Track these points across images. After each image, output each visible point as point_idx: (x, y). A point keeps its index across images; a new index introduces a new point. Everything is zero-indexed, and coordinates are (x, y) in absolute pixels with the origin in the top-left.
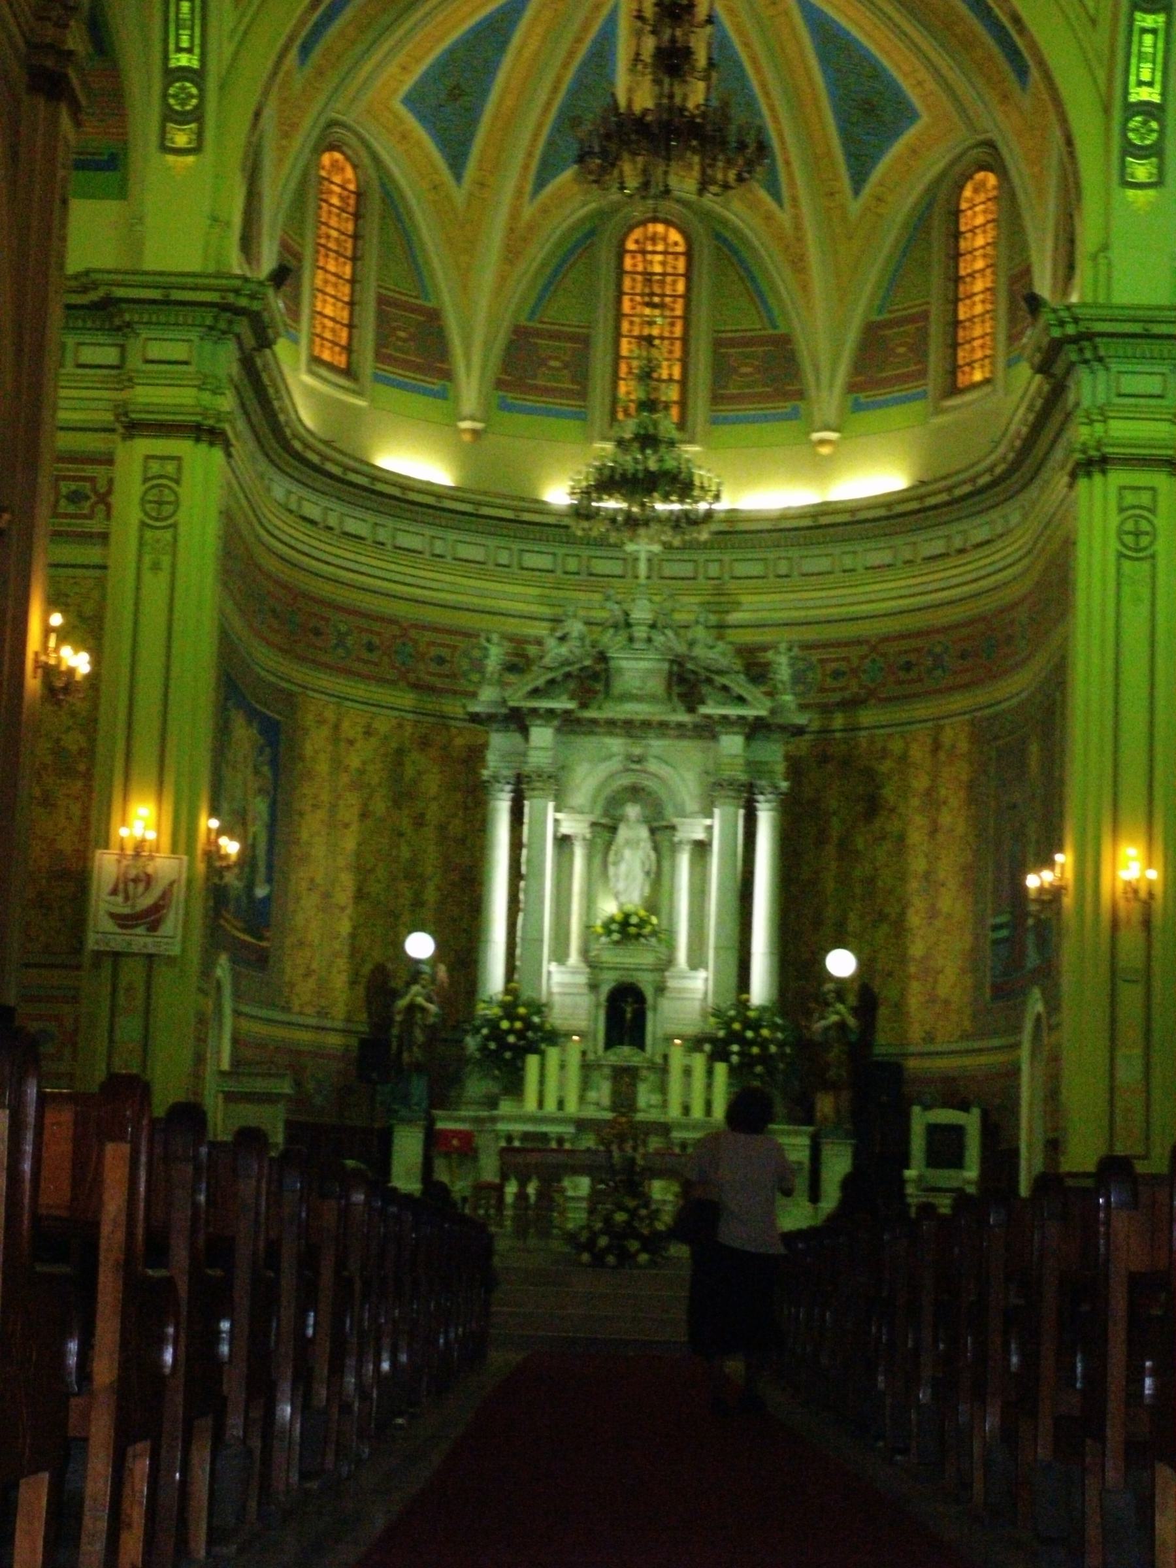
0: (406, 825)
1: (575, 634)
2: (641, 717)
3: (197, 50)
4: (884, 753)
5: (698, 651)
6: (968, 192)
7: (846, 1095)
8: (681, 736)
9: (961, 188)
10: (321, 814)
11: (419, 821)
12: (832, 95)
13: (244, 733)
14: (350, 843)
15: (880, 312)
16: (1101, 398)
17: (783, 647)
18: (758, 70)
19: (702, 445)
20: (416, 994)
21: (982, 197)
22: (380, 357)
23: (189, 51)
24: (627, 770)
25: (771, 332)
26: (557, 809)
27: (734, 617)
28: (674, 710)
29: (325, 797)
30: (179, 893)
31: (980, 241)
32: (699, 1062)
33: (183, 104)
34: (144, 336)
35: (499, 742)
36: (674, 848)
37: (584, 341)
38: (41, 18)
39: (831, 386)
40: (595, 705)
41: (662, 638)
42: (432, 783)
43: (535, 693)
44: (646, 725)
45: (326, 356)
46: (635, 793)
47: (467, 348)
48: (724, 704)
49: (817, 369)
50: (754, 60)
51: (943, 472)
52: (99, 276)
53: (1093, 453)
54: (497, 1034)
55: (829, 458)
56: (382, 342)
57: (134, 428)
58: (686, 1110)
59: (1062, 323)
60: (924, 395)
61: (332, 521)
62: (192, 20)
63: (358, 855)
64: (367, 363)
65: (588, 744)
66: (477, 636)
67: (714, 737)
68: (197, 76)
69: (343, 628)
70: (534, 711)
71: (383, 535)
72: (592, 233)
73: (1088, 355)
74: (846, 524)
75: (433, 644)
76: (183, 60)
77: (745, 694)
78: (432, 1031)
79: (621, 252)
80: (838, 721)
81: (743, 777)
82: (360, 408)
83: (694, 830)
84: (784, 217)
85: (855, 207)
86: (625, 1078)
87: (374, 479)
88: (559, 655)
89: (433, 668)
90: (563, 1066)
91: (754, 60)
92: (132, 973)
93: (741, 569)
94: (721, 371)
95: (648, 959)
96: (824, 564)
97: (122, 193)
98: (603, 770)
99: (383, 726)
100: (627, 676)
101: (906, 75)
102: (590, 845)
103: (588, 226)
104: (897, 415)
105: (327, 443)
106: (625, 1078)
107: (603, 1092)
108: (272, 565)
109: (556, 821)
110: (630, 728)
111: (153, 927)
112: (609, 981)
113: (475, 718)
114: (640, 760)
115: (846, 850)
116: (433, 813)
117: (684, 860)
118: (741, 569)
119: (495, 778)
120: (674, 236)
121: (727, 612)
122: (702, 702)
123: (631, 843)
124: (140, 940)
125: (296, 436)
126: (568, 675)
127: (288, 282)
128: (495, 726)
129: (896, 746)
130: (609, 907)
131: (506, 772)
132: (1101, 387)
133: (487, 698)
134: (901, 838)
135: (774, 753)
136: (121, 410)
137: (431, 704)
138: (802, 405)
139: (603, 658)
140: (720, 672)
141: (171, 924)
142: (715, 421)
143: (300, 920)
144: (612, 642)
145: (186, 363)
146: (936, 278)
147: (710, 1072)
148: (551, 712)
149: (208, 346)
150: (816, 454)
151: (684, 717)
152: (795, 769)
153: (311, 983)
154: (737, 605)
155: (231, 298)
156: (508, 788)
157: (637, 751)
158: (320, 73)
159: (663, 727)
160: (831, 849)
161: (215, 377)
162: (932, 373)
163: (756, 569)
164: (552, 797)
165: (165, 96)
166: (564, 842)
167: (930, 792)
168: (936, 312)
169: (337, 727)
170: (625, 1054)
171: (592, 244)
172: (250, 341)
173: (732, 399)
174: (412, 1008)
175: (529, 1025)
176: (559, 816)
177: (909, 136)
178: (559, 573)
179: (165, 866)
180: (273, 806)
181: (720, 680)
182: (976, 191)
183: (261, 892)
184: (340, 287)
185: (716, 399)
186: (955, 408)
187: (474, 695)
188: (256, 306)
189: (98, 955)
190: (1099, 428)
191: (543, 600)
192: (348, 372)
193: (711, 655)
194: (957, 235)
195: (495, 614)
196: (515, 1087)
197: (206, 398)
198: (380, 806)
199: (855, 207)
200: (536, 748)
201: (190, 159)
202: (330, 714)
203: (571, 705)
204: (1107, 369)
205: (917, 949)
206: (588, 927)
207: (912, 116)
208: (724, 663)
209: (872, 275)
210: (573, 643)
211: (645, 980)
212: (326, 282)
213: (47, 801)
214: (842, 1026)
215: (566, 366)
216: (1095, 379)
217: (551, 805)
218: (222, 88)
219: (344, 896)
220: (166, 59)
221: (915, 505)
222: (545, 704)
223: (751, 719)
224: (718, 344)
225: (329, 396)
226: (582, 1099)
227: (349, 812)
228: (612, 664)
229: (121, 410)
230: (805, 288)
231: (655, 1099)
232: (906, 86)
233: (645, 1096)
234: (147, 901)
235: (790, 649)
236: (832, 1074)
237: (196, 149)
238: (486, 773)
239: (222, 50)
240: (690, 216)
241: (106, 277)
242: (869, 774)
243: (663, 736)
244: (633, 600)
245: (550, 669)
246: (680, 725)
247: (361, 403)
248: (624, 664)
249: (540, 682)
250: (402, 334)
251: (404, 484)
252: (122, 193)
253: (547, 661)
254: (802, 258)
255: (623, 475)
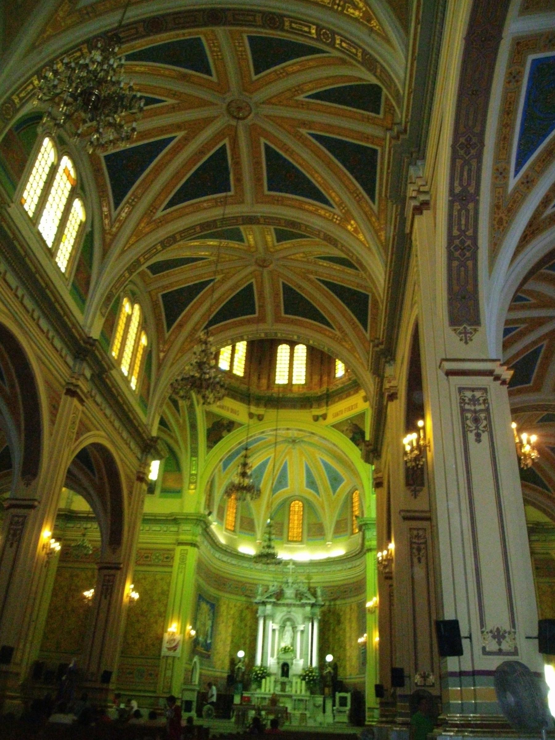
0: (243, 626)
4: (341, 611)
7: (331, 689)
10: (224, 624)
11: (246, 625)
13: (205, 607)
14: (230, 630)
20: (240, 665)
27: (312, 581)
29: (225, 621)
30: (181, 643)
32: (299, 680)
35: (261, 608)
36: (297, 632)
42: (249, 617)
43: (268, 598)
46: (289, 619)
54: (257, 674)
55: (330, 548)
57: (180, 544)
58: (296, 692)
63: (232, 633)
65: (280, 608)
67: (265, 605)
68: (196, 475)
71: (240, 564)
76: (193, 472)
78: (244, 673)
80: (332, 603)
81: (310, 616)
83: (301, 627)
84: (321, 499)
86: (283, 684)
90: (270, 682)
92: (170, 661)
94: (309, 530)
95: (290, 657)
99: (238, 604)
102: (279, 631)
106: (283, 684)
107: (279, 688)
108: (214, 571)
110: (288, 605)
111: (175, 650)
112: (282, 662)
113: (256, 603)
114: (290, 612)
115: (334, 631)
116: (249, 624)
117: (299, 634)
123: (289, 631)
124: (171, 653)
129: (343, 609)
130: (283, 645)
133: (258, 599)
134: (345, 630)
135: (317, 611)
136: (177, 540)
137: (249, 600)
141: (179, 650)
142: (308, 540)
143: (218, 647)
144: (284, 587)
146: (349, 510)
147: (301, 683)
151: (298, 603)
152: (324, 614)
153: (220, 662)
158: (227, 474)
159: (294, 605)
160: (331, 632)
166: (274, 630)
167: (350, 618)
168: (349, 517)
169: (228, 605)
170: (285, 679)
172: (204, 527)
174: (239, 668)
175: (264, 672)
179: (178, 637)
180: (213, 622)
183: (209, 641)
185: (308, 536)
189: (164, 657)
192: (234, 531)
194: (352, 503)
196: (260, 686)
197: (194, 538)
198: (237, 622)
202: (227, 602)
205: (348, 654)
206: (278, 649)
207: (343, 480)
209: (337, 511)
211: (289, 662)
213: (156, 622)
214: (330, 672)
219: (229, 642)
226: (274, 689)
227: (230, 623)
229: (177, 540)
231: (290, 689)
233: (288, 688)
234: (174, 645)
236: (328, 683)
238: (258, 615)
242: (338, 615)
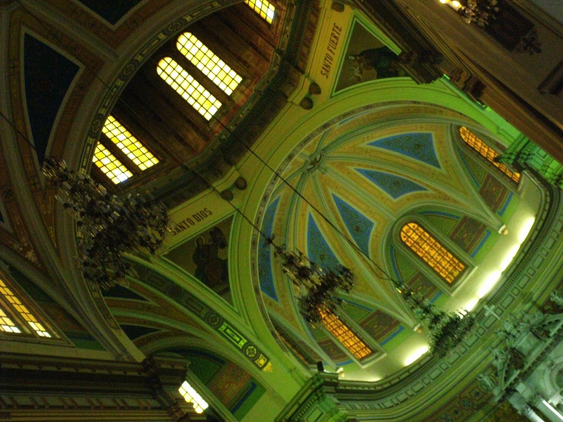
1: (498, 353)
2: (540, 353)
3: (242, 338)
5: (533, 322)
6: (463, 137)
8: (555, 346)
9: (461, 137)
12: (405, 153)
15: (478, 186)
16: (541, 163)
17: (552, 294)
18: (382, 169)
19: (476, 265)
21: (468, 134)
22: (376, 339)
23: (241, 339)
24: (552, 370)
25: (460, 221)
26: (547, 400)
27: (534, 298)
28: (545, 341)
31: (479, 144)
33: (253, 353)
34: (305, 419)
35: (513, 400)
37: (420, 274)
38: (172, 414)
39: (488, 216)
40: (525, 364)
41: (521, 327)
43: (506, 379)
44: (543, 354)
45: (363, 355)
47: (396, 311)
48: (555, 327)
49: (481, 217)
50: (379, 168)
51: (537, 207)
52: (279, 418)
53: (555, 178)
56: (372, 334)
59: (509, 158)
60: (512, 193)
61: (410, 393)
62: (233, 332)
64: (375, 344)
65: (535, 374)
66: (476, 379)
68: (249, 343)
69: (443, 416)
70: (511, 384)
72: (392, 247)
73: (525, 157)
74: (524, 257)
75: (470, 393)
76: (242, 343)
77: (556, 319)
79: (404, 244)
82: (386, 357)
84: (430, 191)
85: (443, 170)
87: (408, 371)
88: (500, 364)
89: (477, 398)
91: (379, 168)
93: (522, 284)
94: (460, 243)
96: (539, 259)
97: (264, 390)
98: (546, 377)
100: (524, 346)
101: (416, 129)
103: (389, 247)
104: (512, 205)
105: (386, 377)
109: (551, 404)
110: (541, 359)
113: (500, 401)
114: (552, 364)
118: (522, 284)
119: (523, 411)
120: (411, 225)
121: (532, 298)
122: (549, 332)
125: (375, 387)
126: (509, 365)
127: (324, 366)
128: (507, 398)
131: (524, 406)
132: (539, 161)
133: (497, 393)
138: (487, 228)
139: (513, 350)
140: (544, 321)
142: (472, 256)
144: (510, 343)
145: (322, 414)
146: (480, 163)
148: (516, 380)
149: (323, 403)
150: (506, 236)
151: (549, 341)
154: (531, 294)
155: (314, 387)
156: (529, 409)
157: (549, 362)
159: (548, 349)
161: (332, 409)
162: (507, 187)
163: (526, 279)
164: (542, 399)
165: (247, 356)
171: (395, 251)
172: (331, 389)
173: (471, 245)
176: (550, 402)
177: (434, 141)
178: (480, 337)
181: (546, 323)
182: (464, 135)
184: (348, 334)
185: (467, 251)
186: (523, 187)
187: (492, 396)
188: (322, 381)
190: (549, 170)
191: (484, 349)
192: (373, 352)
193: (536, 319)
194: (473, 149)
195: (477, 366)
199: (443, 170)
200: (523, 392)
201: (269, 364)
203: (518, 372)
204: (534, 154)
207: (429, 135)
208: (542, 317)
209: (467, 181)
210: (500, 356)
212: (343, 337)
215: (423, 286)
216: (535, 160)
217: (544, 402)
218: (258, 338)
220: (238, 348)
221: (541, 223)
222: (512, 379)
223: (561, 328)
224: (451, 238)
225: (374, 364)
228: (517, 348)
230: (455, 201)
232: (419, 131)
235: (555, 293)
237: (268, 360)
238: (519, 412)
239: (247, 330)
240: (409, 216)
241: (281, 417)
243: (550, 351)
244: (503, 326)
245: (502, 369)
246: (551, 344)
247: (385, 355)
248: (519, 345)
249: (504, 375)
250: (375, 327)
251: (418, 362)
252: (264, 390)
253: (499, 368)
254: (446, 196)
255: (441, 335)
